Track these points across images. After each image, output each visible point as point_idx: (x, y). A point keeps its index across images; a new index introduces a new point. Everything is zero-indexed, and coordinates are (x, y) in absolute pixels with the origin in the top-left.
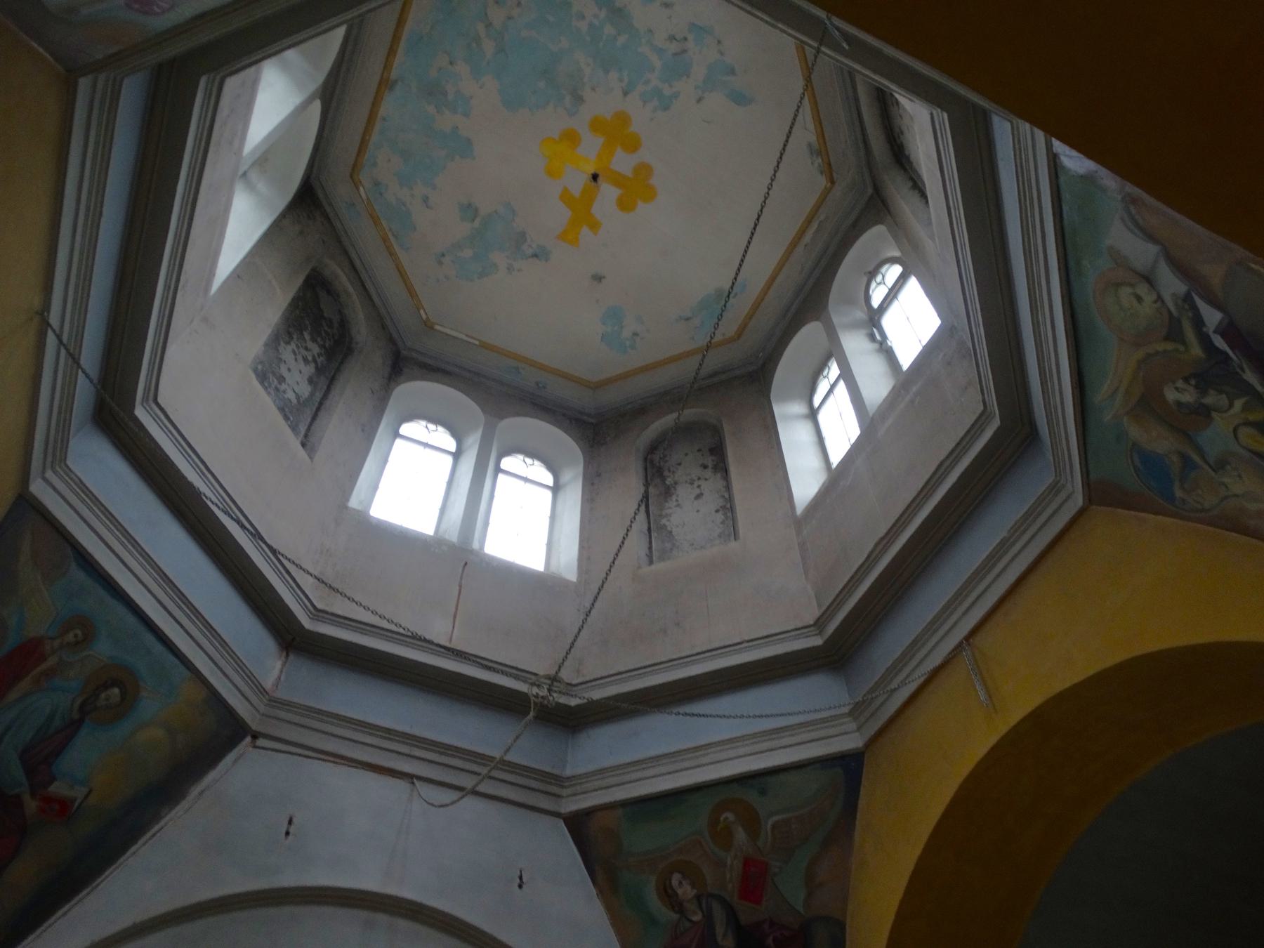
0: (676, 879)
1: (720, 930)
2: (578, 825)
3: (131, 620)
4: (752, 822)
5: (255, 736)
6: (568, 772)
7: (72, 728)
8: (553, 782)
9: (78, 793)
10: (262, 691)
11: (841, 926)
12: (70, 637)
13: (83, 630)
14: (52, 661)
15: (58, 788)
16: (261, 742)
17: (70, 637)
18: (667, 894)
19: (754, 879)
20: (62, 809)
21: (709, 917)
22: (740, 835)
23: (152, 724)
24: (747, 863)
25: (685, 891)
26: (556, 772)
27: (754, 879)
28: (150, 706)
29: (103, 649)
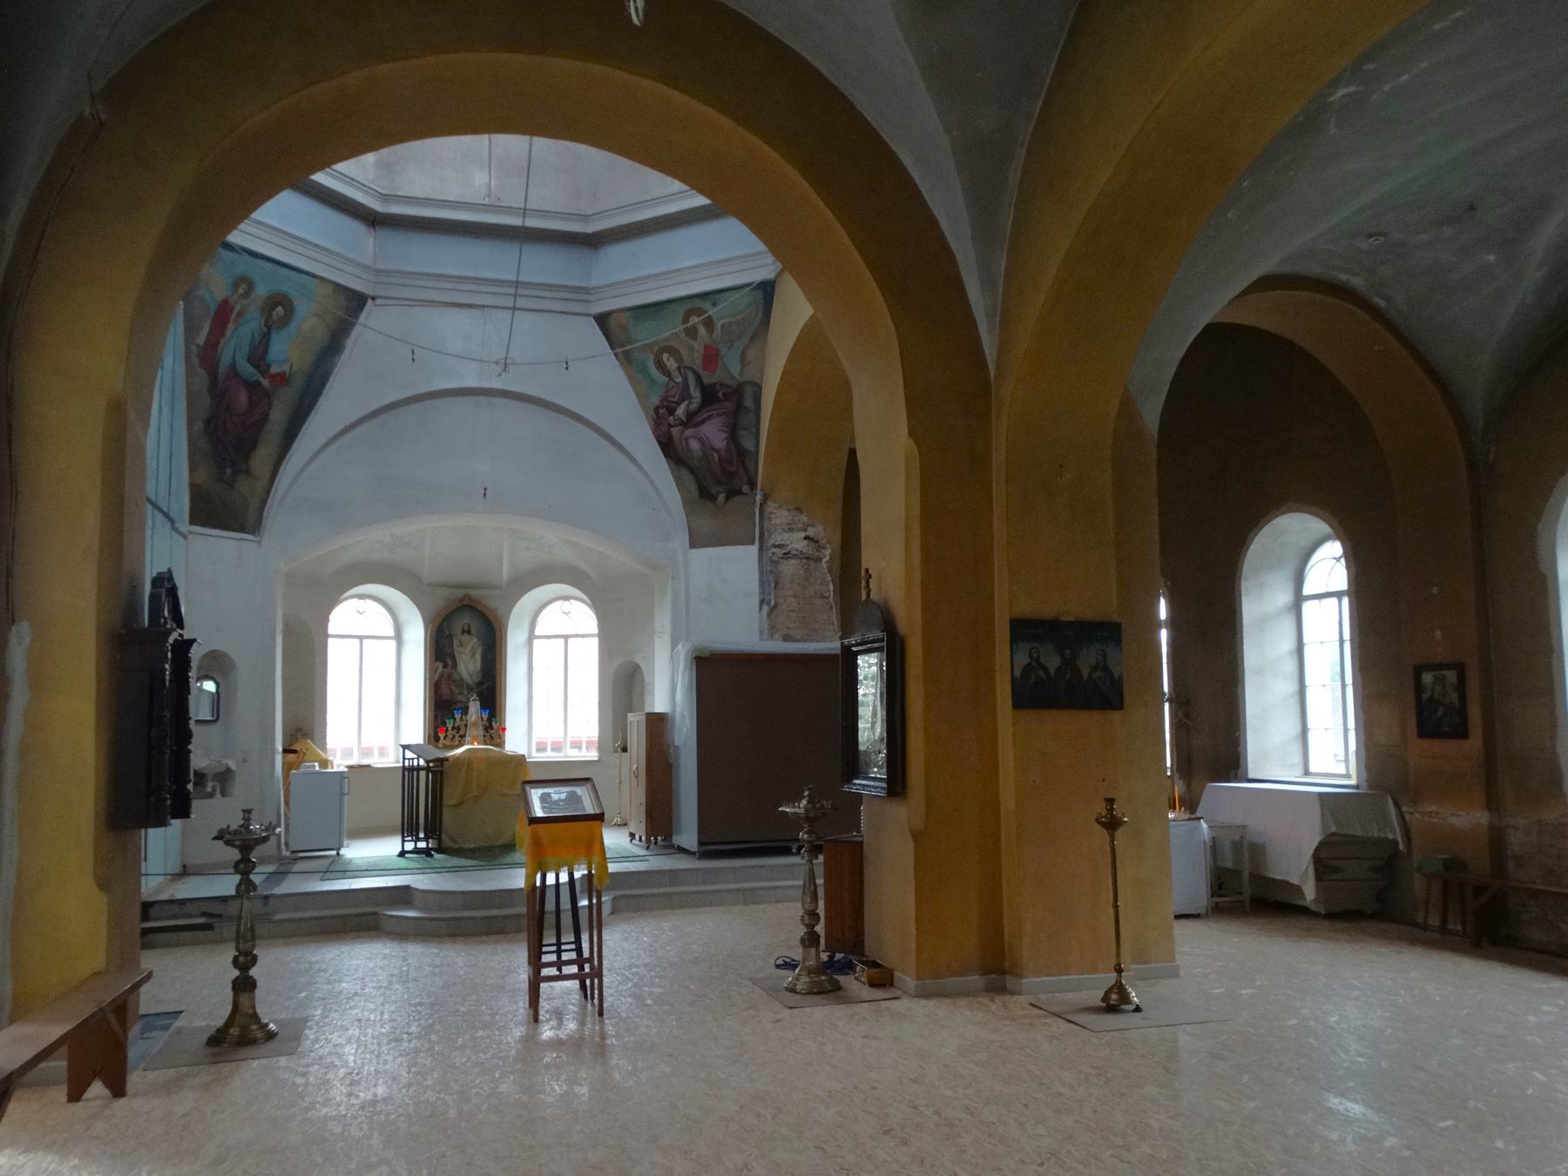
0: (665, 356)
1: (692, 388)
2: (602, 320)
3: (269, 265)
4: (709, 323)
5: (373, 298)
6: (594, 283)
7: (266, 337)
8: (583, 292)
9: (286, 368)
10: (366, 268)
11: (760, 387)
12: (241, 291)
13: (244, 284)
14: (238, 307)
15: (274, 370)
16: (378, 301)
17: (241, 291)
18: (661, 366)
19: (711, 357)
20: (282, 379)
21: (685, 379)
22: (702, 331)
23: (309, 320)
24: (707, 347)
25: (671, 364)
26: (583, 284)
27: (711, 357)
28: (302, 308)
29: (262, 290)
